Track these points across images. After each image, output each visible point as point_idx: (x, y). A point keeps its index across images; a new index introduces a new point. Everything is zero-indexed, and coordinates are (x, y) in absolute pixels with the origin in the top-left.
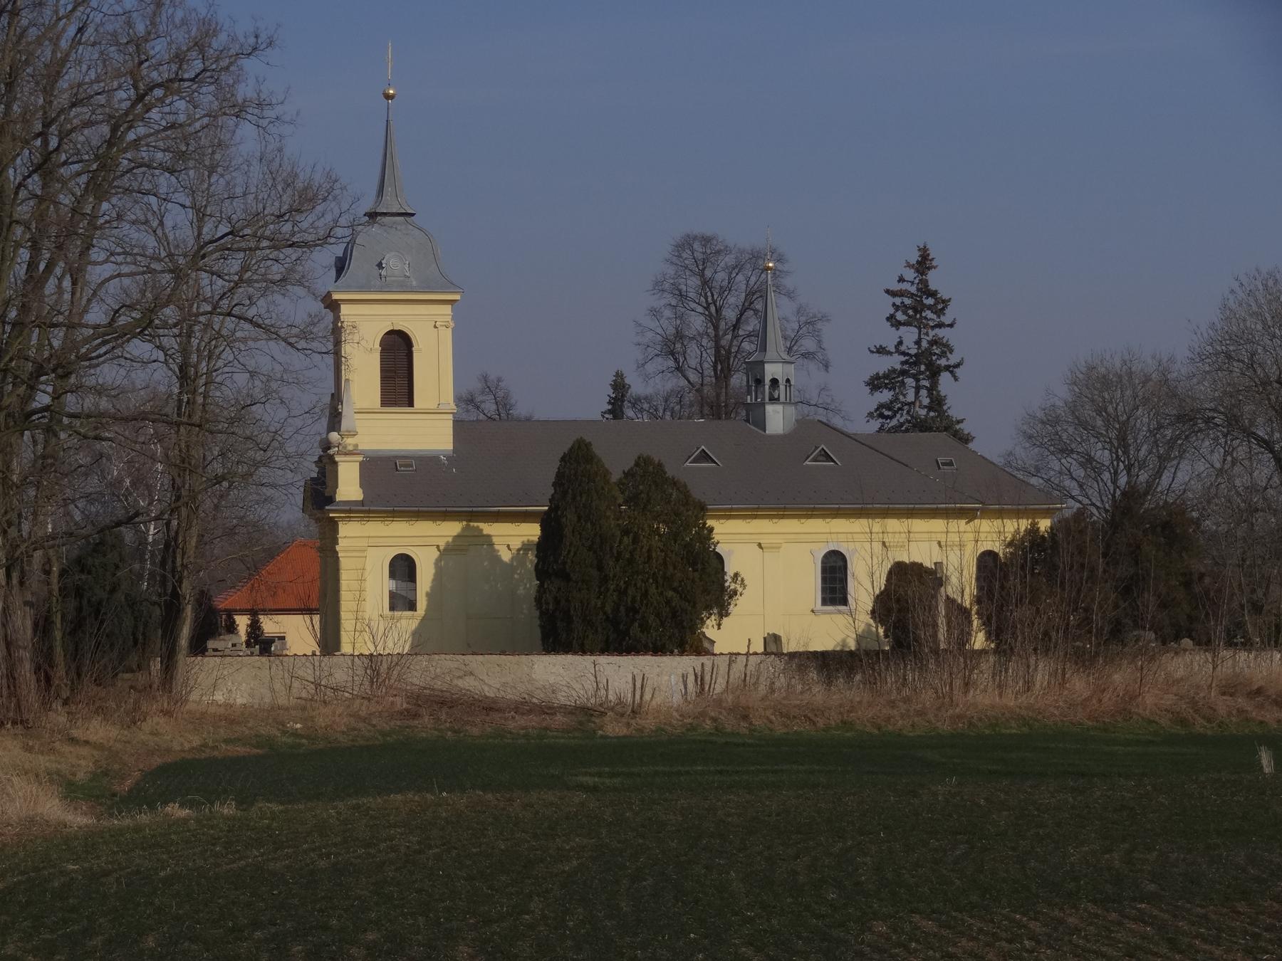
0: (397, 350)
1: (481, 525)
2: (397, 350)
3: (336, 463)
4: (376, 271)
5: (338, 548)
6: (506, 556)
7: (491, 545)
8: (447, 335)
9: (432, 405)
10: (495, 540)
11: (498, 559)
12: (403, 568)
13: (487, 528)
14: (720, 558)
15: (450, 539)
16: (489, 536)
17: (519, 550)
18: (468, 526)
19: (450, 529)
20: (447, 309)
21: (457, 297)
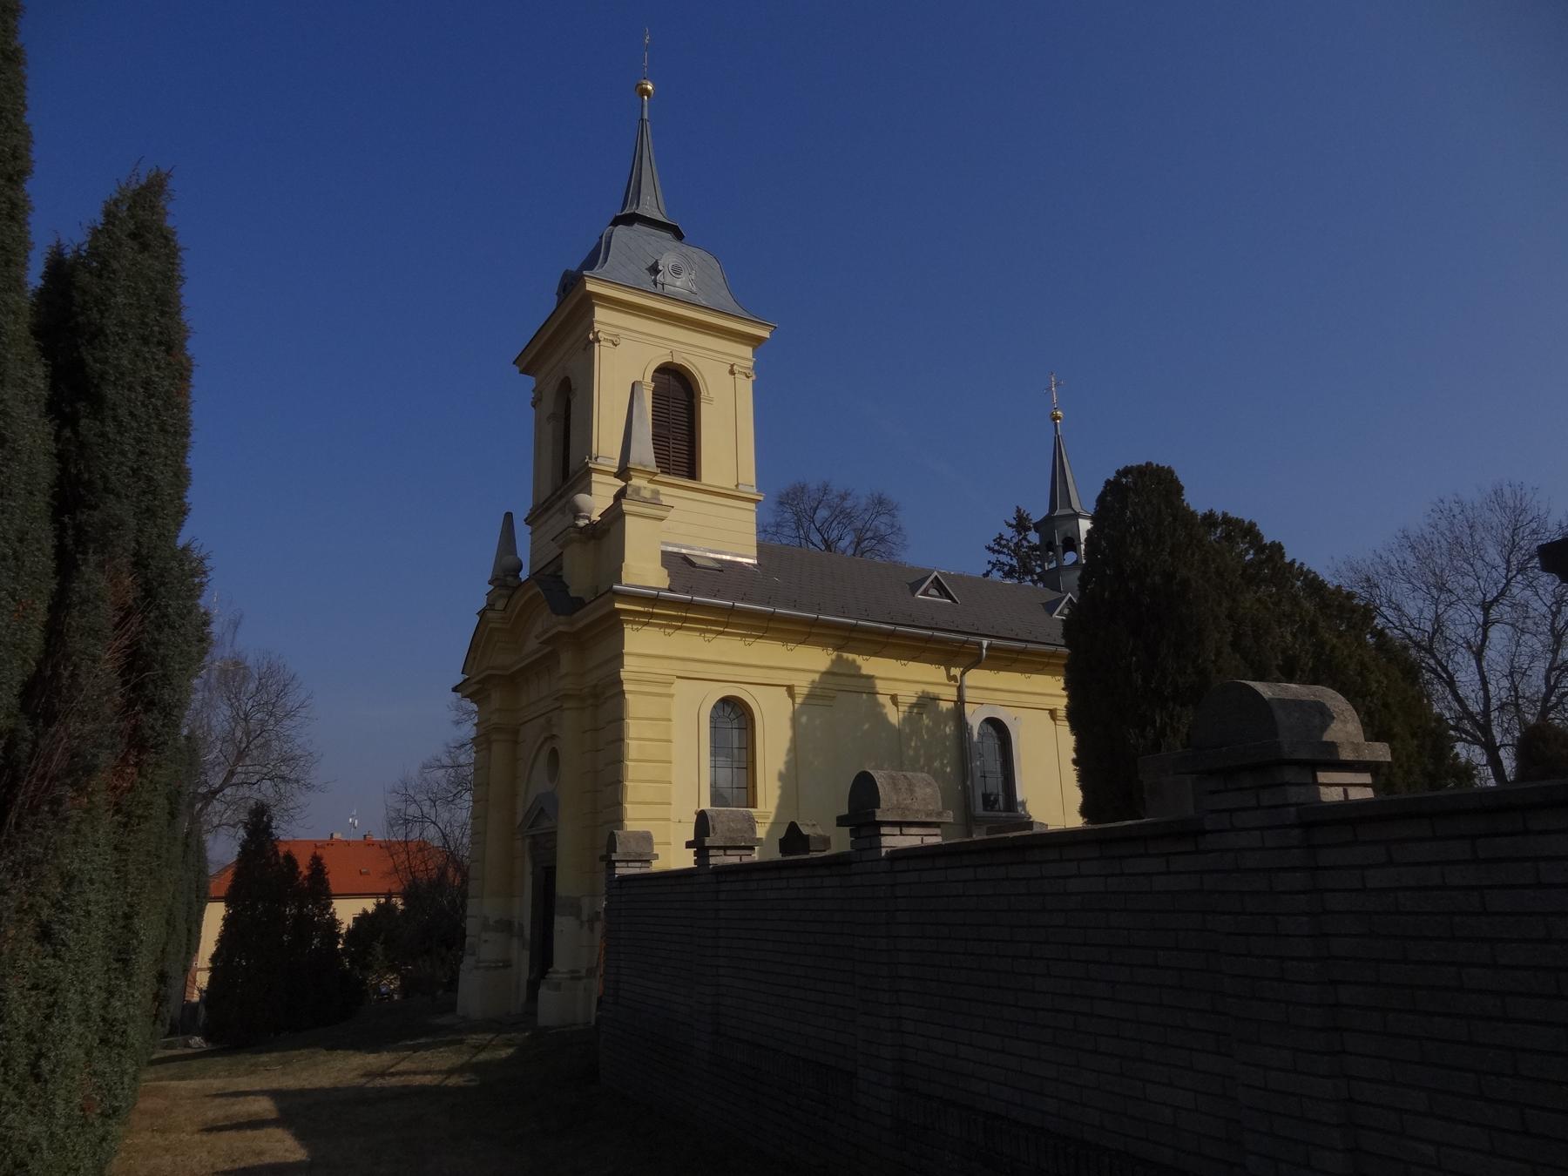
0: (676, 394)
1: (859, 660)
2: (676, 394)
3: (1064, 636)
4: (649, 278)
5: (623, 675)
6: (894, 716)
7: (874, 693)
8: (746, 387)
9: (728, 483)
10: (880, 686)
11: (883, 719)
12: (734, 718)
13: (871, 665)
14: (183, 512)
15: (816, 677)
16: (871, 677)
17: (912, 706)
18: (839, 657)
19: (814, 660)
20: (747, 351)
21: (766, 334)
